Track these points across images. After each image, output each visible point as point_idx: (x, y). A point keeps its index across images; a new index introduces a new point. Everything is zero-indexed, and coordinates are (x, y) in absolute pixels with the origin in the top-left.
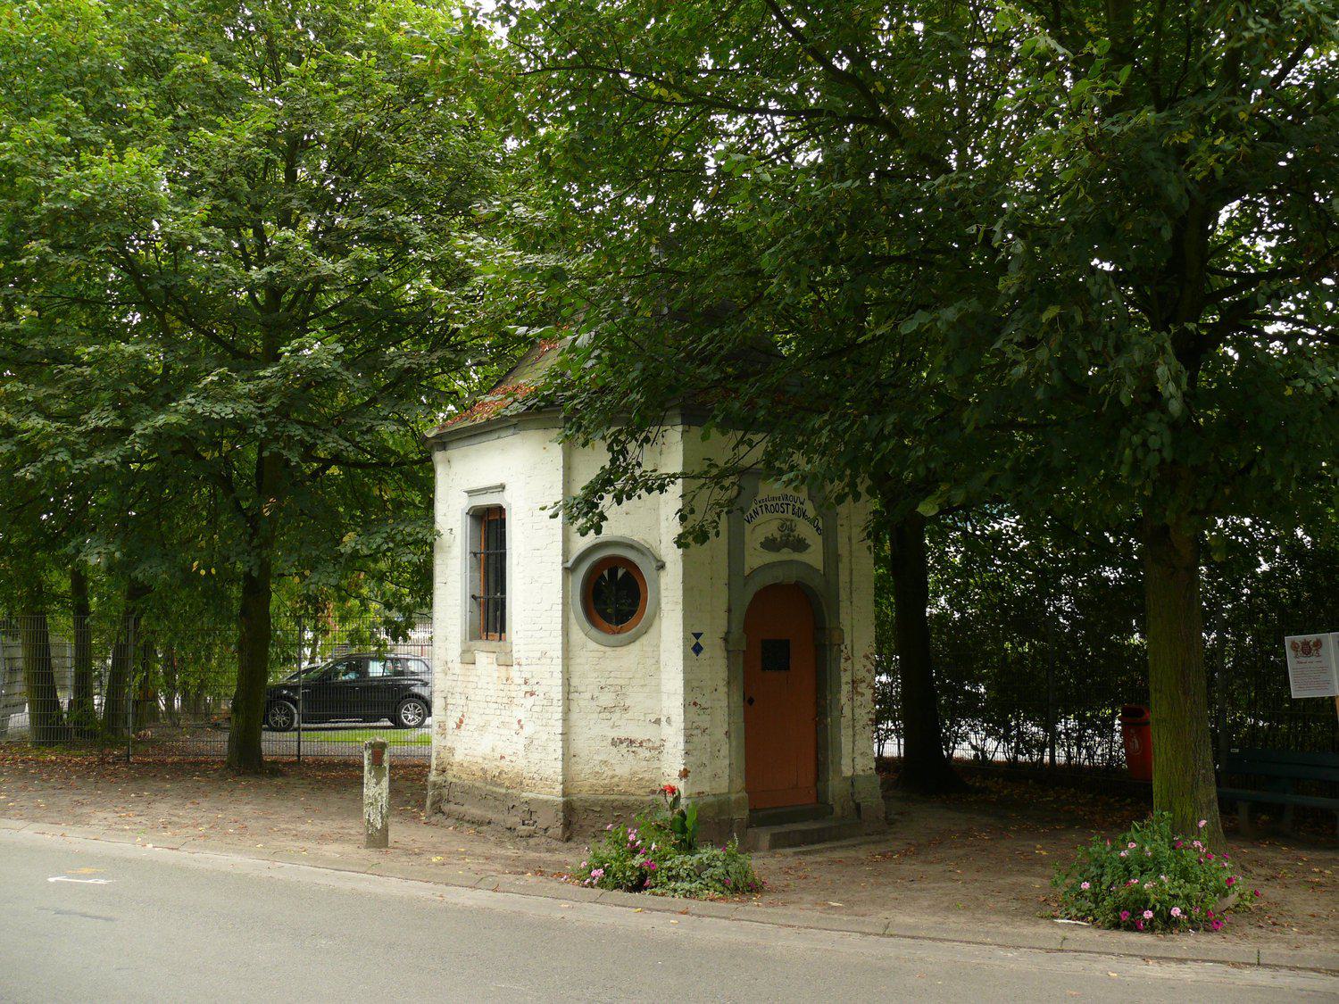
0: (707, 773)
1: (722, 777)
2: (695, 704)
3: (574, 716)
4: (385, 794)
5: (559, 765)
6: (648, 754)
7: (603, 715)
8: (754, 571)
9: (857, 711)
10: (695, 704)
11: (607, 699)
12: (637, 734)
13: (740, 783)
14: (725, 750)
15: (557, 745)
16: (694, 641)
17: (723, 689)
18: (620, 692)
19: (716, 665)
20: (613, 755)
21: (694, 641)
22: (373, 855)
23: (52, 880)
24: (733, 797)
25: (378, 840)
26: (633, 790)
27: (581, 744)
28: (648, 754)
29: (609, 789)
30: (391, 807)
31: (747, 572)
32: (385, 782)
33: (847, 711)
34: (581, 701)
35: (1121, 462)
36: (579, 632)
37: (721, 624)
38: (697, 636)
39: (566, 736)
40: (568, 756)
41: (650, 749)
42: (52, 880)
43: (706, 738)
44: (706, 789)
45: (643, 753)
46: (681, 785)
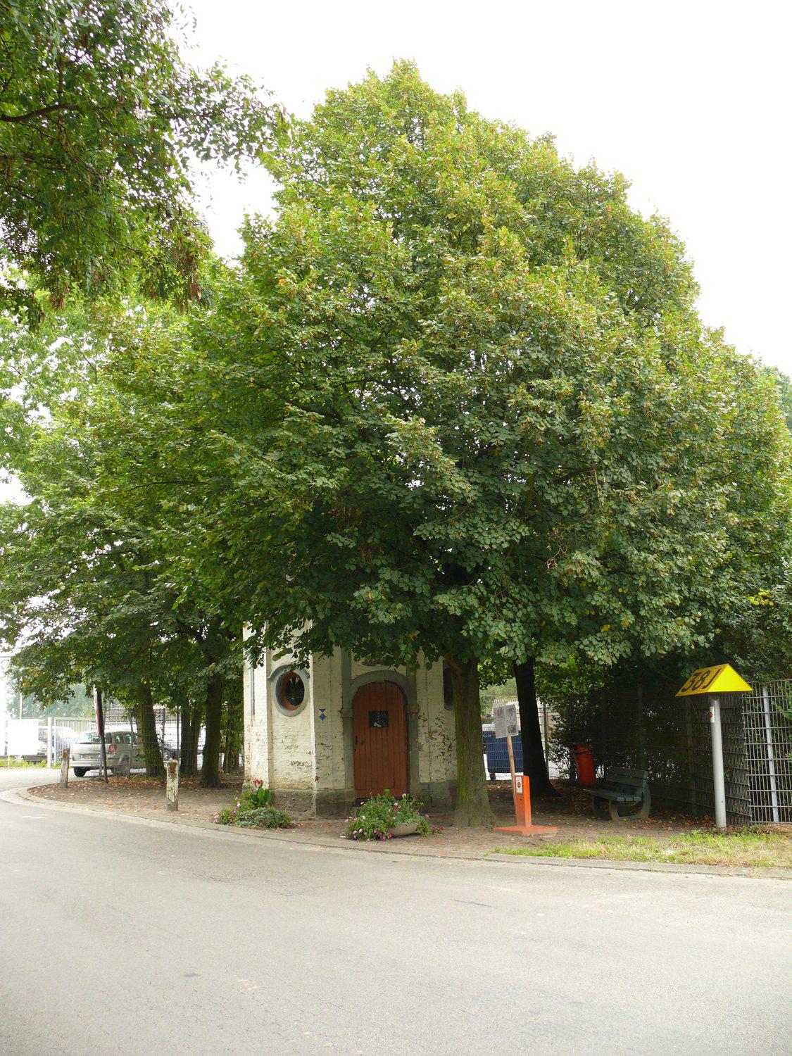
0: (330, 778)
1: (340, 780)
2: (322, 744)
3: (275, 751)
4: (177, 785)
5: (267, 774)
6: (306, 769)
7: (287, 750)
8: (358, 677)
9: (432, 748)
10: (322, 744)
11: (288, 742)
12: (302, 760)
13: (351, 784)
14: (342, 767)
15: (266, 765)
16: (320, 713)
17: (340, 737)
18: (294, 739)
19: (336, 726)
20: (291, 769)
21: (320, 713)
22: (172, 815)
23: (485, 756)
24: (346, 791)
25: (174, 807)
26: (300, 787)
27: (277, 765)
28: (306, 769)
29: (290, 787)
30: (179, 793)
31: (353, 676)
32: (176, 781)
33: (425, 748)
34: (277, 743)
35: (266, 371)
36: (276, 709)
37: (338, 704)
38: (323, 710)
39: (271, 760)
40: (271, 770)
41: (307, 767)
42: (485, 756)
43: (329, 761)
44: (330, 786)
45: (305, 769)
46: (315, 784)
